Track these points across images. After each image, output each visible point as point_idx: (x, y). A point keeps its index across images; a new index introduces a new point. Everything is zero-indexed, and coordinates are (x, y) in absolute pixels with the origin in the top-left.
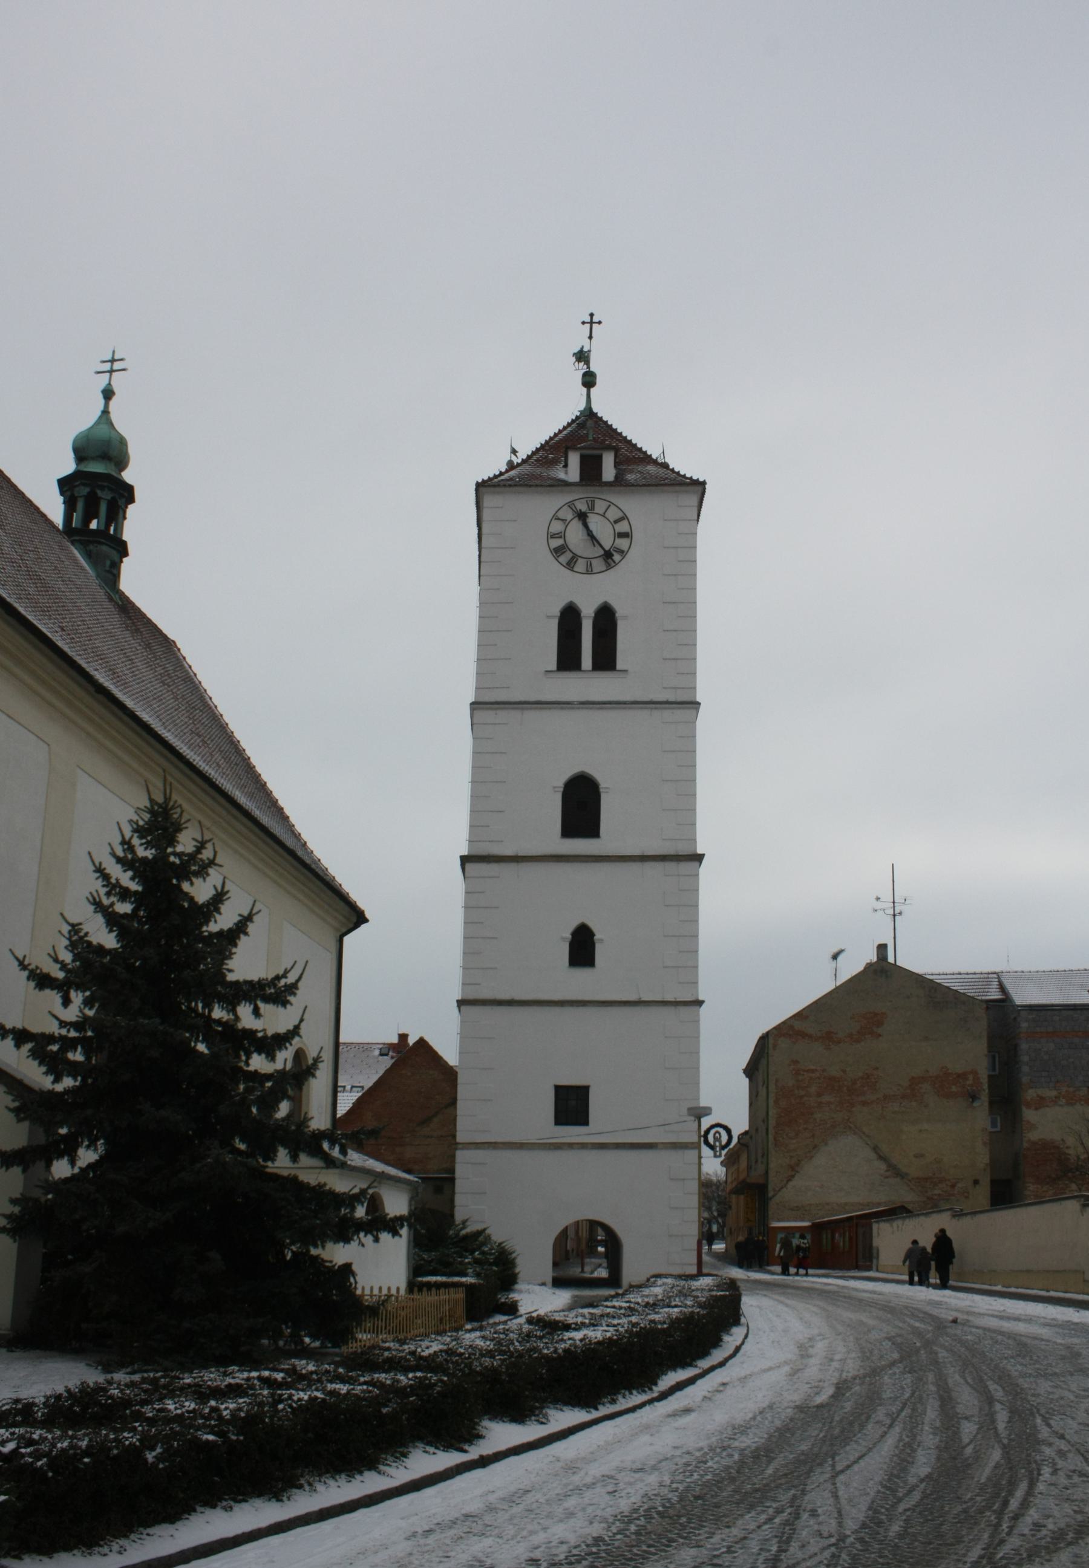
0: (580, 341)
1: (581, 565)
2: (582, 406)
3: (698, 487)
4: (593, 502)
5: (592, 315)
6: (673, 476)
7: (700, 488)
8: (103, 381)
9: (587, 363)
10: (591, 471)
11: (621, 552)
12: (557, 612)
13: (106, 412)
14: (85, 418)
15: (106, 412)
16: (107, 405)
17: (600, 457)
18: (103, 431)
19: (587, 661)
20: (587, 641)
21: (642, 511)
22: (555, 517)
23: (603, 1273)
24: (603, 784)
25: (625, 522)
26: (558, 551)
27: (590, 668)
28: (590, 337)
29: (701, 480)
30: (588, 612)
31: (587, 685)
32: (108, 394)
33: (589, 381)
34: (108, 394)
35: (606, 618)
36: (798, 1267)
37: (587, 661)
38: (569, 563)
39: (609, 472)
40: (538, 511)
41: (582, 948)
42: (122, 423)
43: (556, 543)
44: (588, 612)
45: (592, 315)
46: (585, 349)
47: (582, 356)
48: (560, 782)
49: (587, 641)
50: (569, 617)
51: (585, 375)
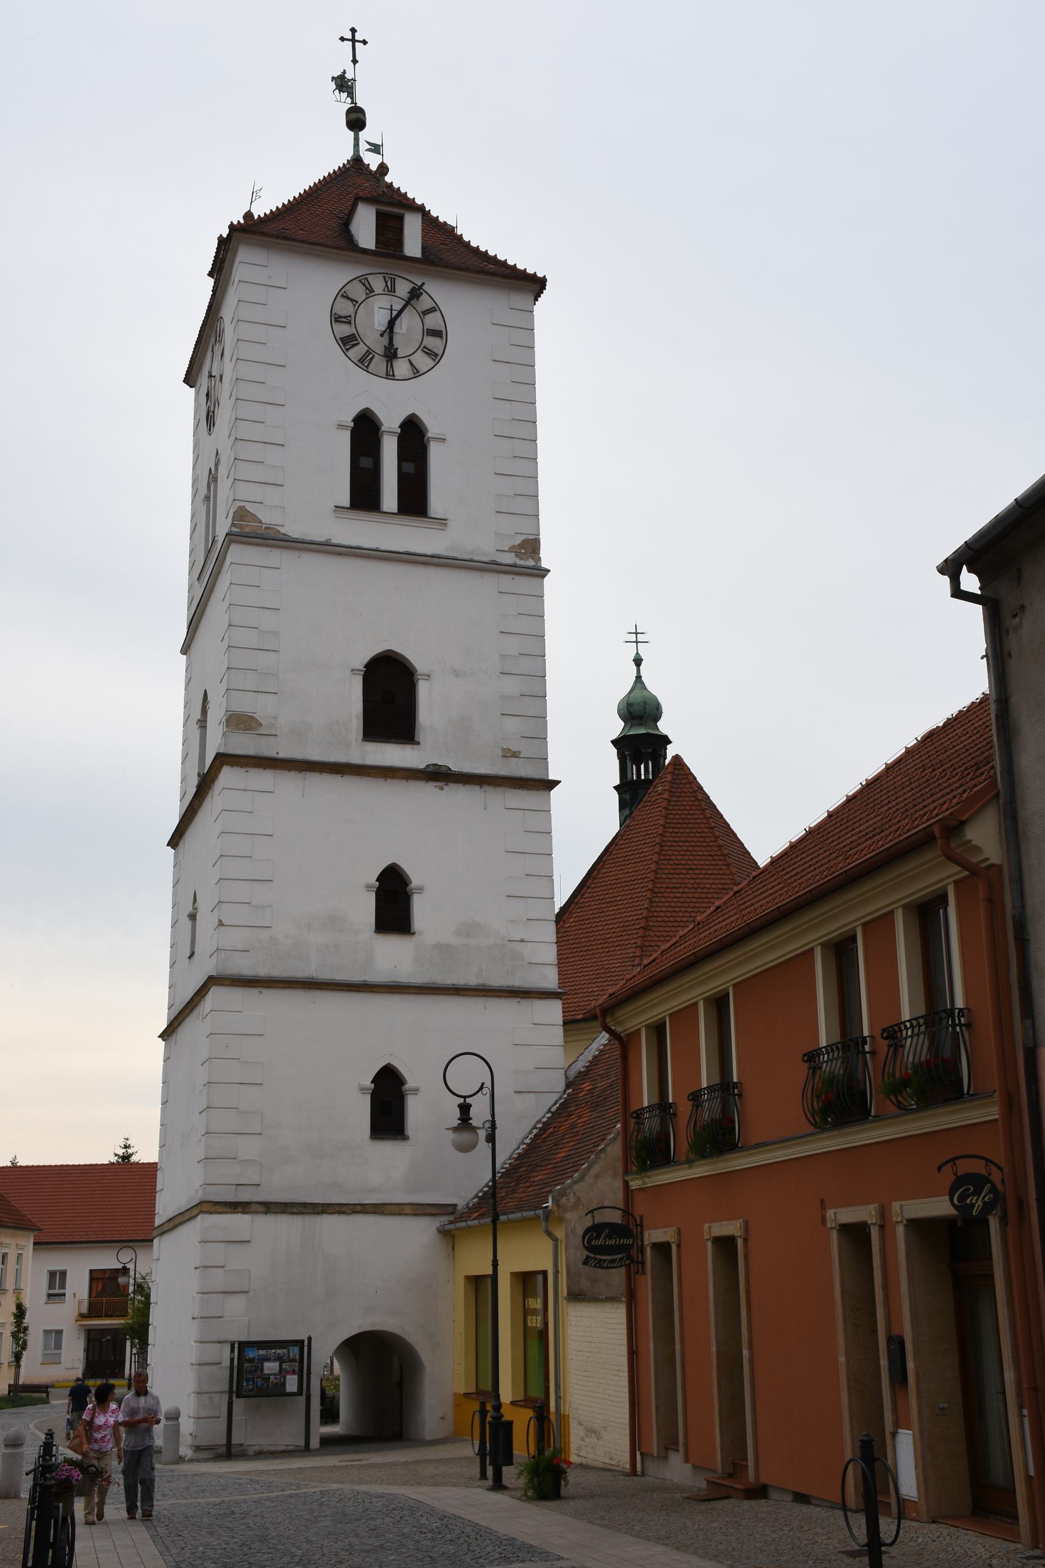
0: (341, 63)
2: (349, 154)
3: (536, 285)
5: (353, 31)
6: (508, 271)
7: (537, 287)
8: (631, 651)
9: (351, 94)
11: (436, 333)
12: (348, 419)
13: (639, 678)
14: (623, 687)
15: (639, 678)
16: (638, 671)
17: (401, 219)
18: (638, 695)
19: (390, 498)
20: (389, 468)
21: (457, 304)
23: (296, 1350)
25: (438, 313)
26: (348, 342)
28: (355, 61)
29: (540, 275)
30: (391, 421)
32: (638, 661)
33: (356, 120)
34: (638, 661)
35: (414, 436)
36: (485, 1193)
37: (390, 498)
38: (362, 361)
40: (305, 290)
41: (394, 902)
42: (653, 686)
43: (345, 330)
44: (391, 421)
45: (353, 31)
46: (349, 76)
47: (343, 84)
48: (372, 878)
49: (389, 468)
50: (365, 430)
51: (349, 112)
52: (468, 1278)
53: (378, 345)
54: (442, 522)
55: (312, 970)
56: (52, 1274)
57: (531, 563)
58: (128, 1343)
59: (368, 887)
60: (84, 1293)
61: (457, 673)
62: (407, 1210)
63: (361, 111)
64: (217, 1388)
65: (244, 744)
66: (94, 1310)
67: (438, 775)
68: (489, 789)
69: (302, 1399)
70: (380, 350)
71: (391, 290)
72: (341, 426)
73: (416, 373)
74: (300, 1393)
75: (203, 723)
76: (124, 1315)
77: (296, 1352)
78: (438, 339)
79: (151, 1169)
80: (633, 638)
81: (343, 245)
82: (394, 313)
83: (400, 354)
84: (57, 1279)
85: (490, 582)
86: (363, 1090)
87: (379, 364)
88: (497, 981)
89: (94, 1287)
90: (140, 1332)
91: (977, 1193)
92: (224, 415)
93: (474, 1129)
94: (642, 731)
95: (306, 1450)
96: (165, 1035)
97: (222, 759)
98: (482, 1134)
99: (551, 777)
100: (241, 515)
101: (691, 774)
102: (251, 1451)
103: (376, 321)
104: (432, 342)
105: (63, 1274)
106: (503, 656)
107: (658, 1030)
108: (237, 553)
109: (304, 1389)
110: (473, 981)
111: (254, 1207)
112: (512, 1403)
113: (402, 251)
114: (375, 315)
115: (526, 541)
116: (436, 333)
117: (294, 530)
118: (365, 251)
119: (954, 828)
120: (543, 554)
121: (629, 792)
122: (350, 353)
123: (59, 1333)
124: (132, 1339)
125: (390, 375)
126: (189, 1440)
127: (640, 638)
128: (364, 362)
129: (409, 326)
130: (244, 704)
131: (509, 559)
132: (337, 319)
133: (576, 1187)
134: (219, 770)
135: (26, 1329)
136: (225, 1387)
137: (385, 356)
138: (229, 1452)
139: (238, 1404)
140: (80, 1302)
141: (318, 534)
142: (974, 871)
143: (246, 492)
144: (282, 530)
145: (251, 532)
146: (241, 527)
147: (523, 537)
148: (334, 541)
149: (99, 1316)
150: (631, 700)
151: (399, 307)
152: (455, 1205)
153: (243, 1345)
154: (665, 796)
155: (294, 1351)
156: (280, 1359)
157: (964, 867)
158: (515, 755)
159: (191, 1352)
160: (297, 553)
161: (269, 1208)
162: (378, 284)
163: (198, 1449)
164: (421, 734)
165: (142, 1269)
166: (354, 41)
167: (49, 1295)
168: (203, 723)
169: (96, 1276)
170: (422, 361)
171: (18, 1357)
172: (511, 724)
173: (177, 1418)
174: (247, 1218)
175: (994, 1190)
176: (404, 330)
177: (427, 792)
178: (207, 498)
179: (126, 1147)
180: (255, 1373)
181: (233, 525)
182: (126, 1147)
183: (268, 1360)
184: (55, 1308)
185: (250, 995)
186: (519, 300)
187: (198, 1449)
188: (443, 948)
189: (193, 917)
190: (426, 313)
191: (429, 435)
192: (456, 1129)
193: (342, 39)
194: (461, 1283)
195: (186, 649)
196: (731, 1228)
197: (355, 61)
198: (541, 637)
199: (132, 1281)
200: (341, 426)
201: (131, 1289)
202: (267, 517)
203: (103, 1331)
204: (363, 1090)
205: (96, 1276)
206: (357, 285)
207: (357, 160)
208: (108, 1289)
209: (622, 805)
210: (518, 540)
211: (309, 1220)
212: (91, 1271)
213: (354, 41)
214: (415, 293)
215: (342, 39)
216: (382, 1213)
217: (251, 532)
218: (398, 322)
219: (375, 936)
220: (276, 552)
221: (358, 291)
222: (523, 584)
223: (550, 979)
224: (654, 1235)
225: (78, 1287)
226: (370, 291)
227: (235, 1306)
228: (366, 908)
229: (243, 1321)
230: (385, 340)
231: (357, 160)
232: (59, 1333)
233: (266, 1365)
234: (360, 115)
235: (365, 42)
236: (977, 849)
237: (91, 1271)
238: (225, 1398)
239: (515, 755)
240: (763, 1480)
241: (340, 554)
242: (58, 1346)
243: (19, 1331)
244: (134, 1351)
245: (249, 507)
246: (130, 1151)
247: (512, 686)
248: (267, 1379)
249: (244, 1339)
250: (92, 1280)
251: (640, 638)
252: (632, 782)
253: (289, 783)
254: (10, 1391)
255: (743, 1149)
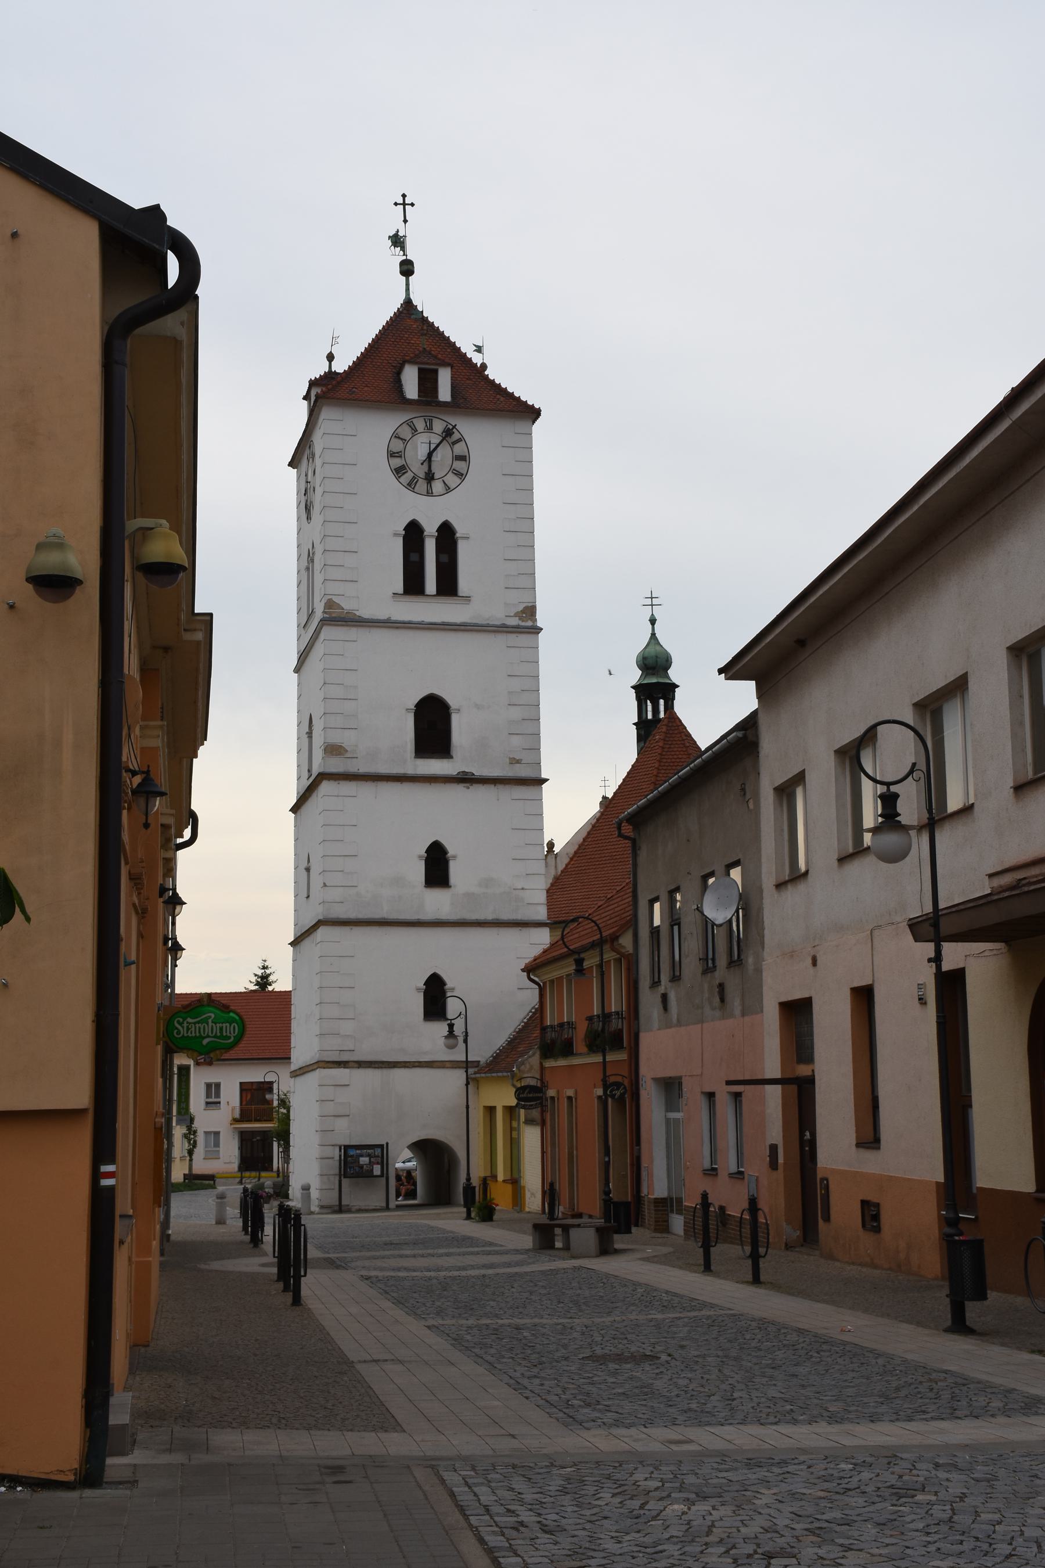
0: (395, 225)
1: (407, 478)
2: (401, 299)
3: (534, 413)
4: (431, 422)
5: (404, 196)
9: (403, 249)
10: (428, 382)
11: (462, 458)
13: (653, 635)
15: (653, 635)
17: (436, 372)
18: (652, 650)
20: (431, 562)
21: (479, 435)
22: (396, 436)
23: (379, 1150)
24: (451, 851)
25: (463, 443)
26: (399, 471)
27: (435, 593)
28: (405, 221)
29: (537, 407)
30: (431, 528)
31: (431, 609)
32: (653, 621)
33: (407, 269)
34: (653, 621)
35: (447, 535)
38: (409, 484)
39: (444, 393)
40: (366, 436)
41: (437, 866)
43: (397, 462)
44: (431, 528)
45: (404, 196)
46: (401, 234)
47: (397, 241)
48: (423, 851)
49: (431, 562)
50: (413, 533)
52: (485, 1107)
53: (421, 471)
54: (467, 599)
55: (385, 912)
56: (209, 1086)
57: (529, 623)
58: (275, 1144)
59: (420, 857)
60: (236, 1101)
61: (478, 707)
62: (448, 1065)
63: (403, 273)
64: (332, 1172)
65: (336, 765)
66: (245, 1115)
67: (465, 779)
68: (500, 787)
69: (384, 1180)
70: (422, 475)
71: (429, 428)
72: (396, 535)
73: (448, 489)
74: (382, 1176)
75: (310, 734)
76: (270, 1120)
77: (380, 1152)
78: (463, 463)
79: (285, 997)
80: (649, 602)
81: (396, 399)
82: (433, 446)
83: (436, 477)
84: (213, 1090)
85: (501, 640)
86: (418, 989)
87: (422, 485)
88: (505, 916)
89: (244, 1095)
90: (284, 1136)
91: (618, 1089)
92: (315, 513)
93: (455, 1037)
94: (654, 680)
95: (387, 1208)
96: (295, 809)
97: (322, 777)
98: (461, 1039)
99: (544, 776)
100: (330, 604)
101: (682, 724)
102: (353, 1209)
103: (419, 453)
104: (459, 465)
105: (218, 1086)
106: (510, 693)
107: (552, 982)
108: (327, 632)
109: (384, 1174)
110: (490, 917)
111: (351, 1064)
112: (504, 1181)
113: (437, 397)
114: (419, 448)
115: (526, 608)
116: (462, 458)
117: (365, 613)
118: (411, 402)
119: (614, 938)
120: (539, 616)
121: (644, 728)
122: (402, 479)
123: (217, 1134)
124: (278, 1141)
125: (429, 493)
126: (317, 1203)
127: (655, 601)
128: (411, 485)
129: (443, 456)
130: (336, 738)
131: (514, 622)
132: (391, 454)
133: (530, 1060)
134: (320, 782)
135: (195, 1132)
136: (337, 1171)
137: (426, 479)
138: (340, 1209)
139: (345, 1182)
140: (233, 1109)
141: (382, 615)
142: (622, 955)
143: (333, 589)
144: (357, 613)
145: (336, 617)
146: (330, 613)
147: (525, 605)
148: (393, 618)
149: (249, 1121)
150: (646, 655)
151: (438, 441)
152: (479, 1062)
153: (347, 1148)
154: (661, 744)
155: (378, 1151)
156: (369, 1155)
157: (618, 953)
158: (518, 762)
159: (315, 1152)
160: (368, 629)
161: (361, 1064)
162: (420, 425)
163: (322, 1207)
164: (454, 751)
165: (284, 1088)
166: (404, 204)
167: (207, 1103)
168: (310, 734)
169: (244, 1088)
170: (452, 480)
171: (191, 1153)
172: (516, 741)
173: (309, 1189)
174: (347, 1071)
175: (625, 1088)
176: (439, 456)
177: (458, 791)
178: (308, 569)
179: (264, 968)
180: (356, 1164)
181: (324, 612)
182: (264, 968)
183: (362, 1156)
184: (213, 1113)
185: (346, 930)
186: (520, 426)
187: (322, 1207)
188: (469, 895)
189: (308, 870)
190: (454, 443)
191: (458, 535)
192: (446, 1037)
193: (396, 204)
194: (482, 1109)
195: (297, 670)
196: (570, 1093)
197: (405, 221)
198: (537, 677)
199: (276, 1097)
200: (396, 535)
201: (275, 1103)
202: (347, 605)
203: (253, 1133)
204: (418, 989)
205: (244, 1088)
206: (406, 427)
207: (408, 304)
208: (257, 1099)
209: (640, 739)
210: (521, 608)
211: (385, 1071)
212: (241, 1083)
213: (404, 204)
214: (448, 433)
215: (396, 204)
216: (432, 1067)
217: (336, 617)
218: (434, 454)
219: (424, 889)
220: (354, 630)
221: (406, 433)
222: (523, 639)
223: (541, 913)
224: (551, 1093)
225: (231, 1097)
226: (415, 430)
227: (341, 1125)
228: (418, 871)
229: (347, 1133)
230: (425, 467)
231: (408, 304)
232: (217, 1134)
233: (361, 1159)
234: (410, 267)
235: (412, 205)
236: (624, 947)
237: (241, 1083)
238: (337, 1178)
239: (518, 762)
240: (580, 1211)
241: (397, 628)
242: (217, 1144)
243: (190, 1133)
244: (281, 1150)
245: (336, 599)
246: (268, 972)
247: (516, 713)
248: (361, 1167)
249: (347, 1143)
250: (242, 1090)
251: (655, 601)
252: (648, 721)
253: (366, 790)
254: (185, 1179)
255: (576, 1054)
